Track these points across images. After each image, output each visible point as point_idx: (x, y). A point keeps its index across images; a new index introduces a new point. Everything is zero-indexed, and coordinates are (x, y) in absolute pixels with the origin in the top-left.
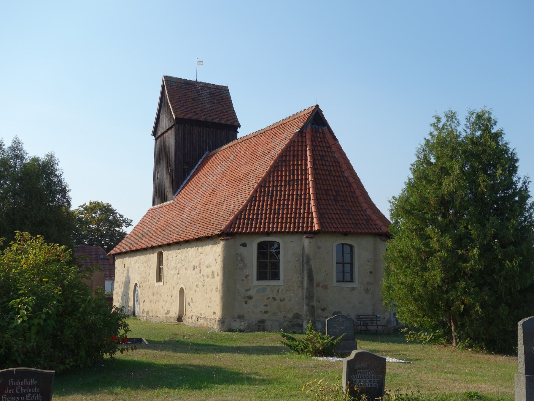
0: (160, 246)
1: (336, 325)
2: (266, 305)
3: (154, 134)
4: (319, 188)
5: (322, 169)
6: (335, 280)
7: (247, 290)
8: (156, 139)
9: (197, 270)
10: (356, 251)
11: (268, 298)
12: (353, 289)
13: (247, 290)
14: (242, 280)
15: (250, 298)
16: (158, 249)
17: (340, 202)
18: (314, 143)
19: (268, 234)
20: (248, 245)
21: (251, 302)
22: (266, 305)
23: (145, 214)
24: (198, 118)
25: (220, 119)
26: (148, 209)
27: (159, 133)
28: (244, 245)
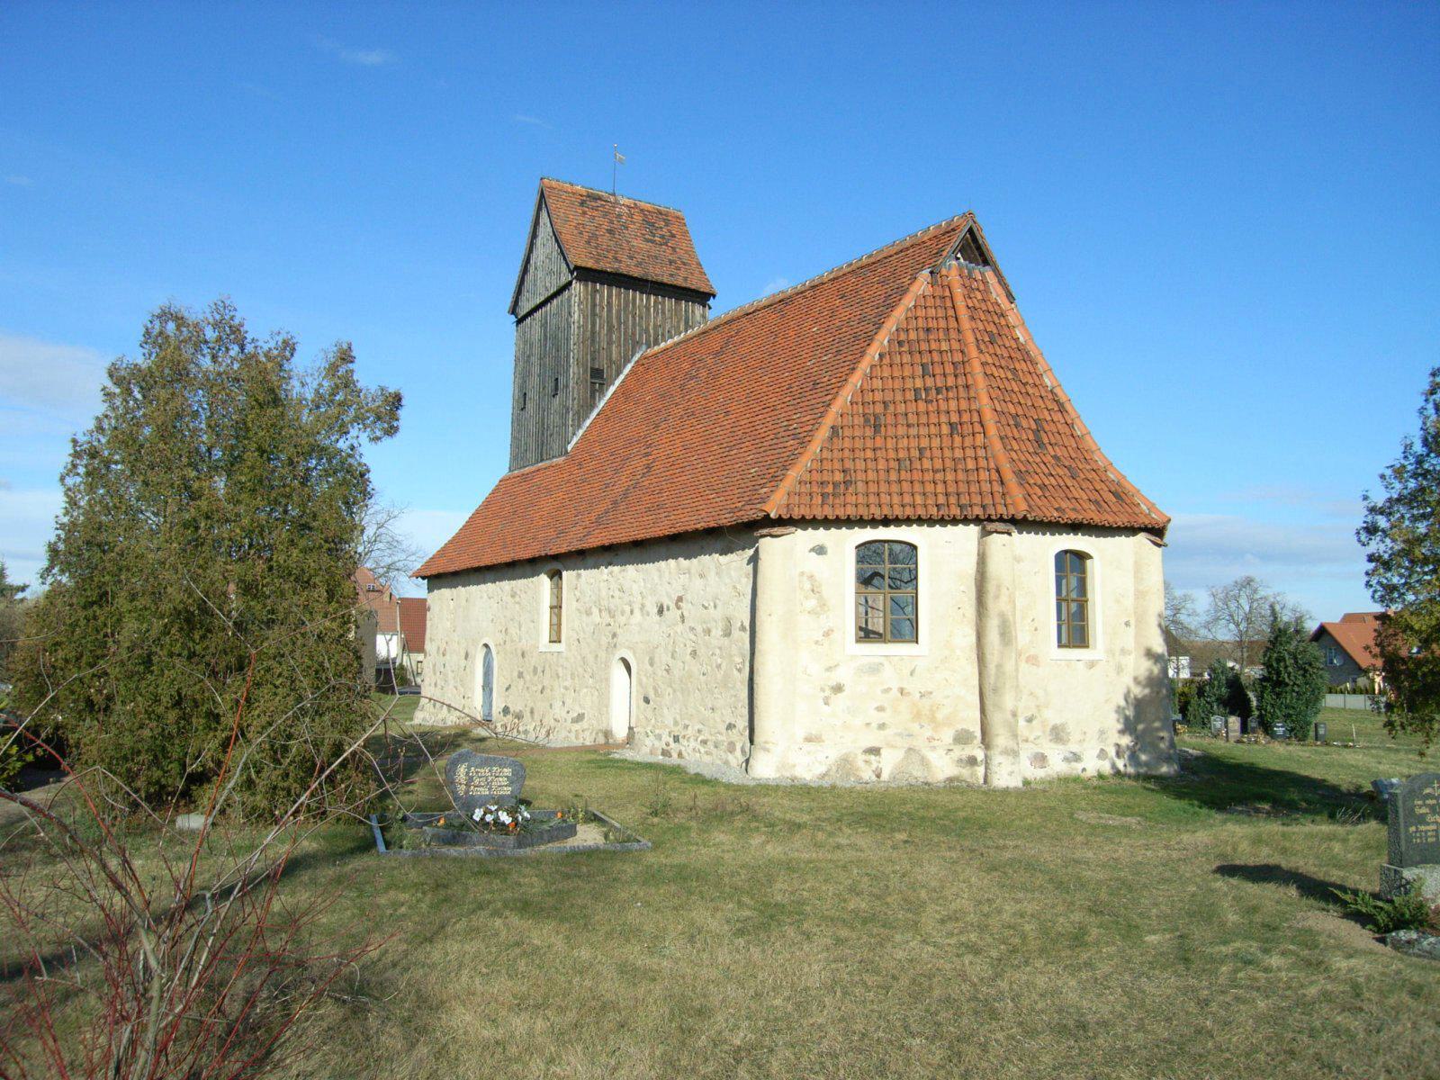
0: (556, 557)
1: (1424, 810)
2: (880, 709)
3: (513, 311)
4: (999, 409)
5: (997, 364)
6: (547, 638)
7: (829, 669)
8: (519, 322)
9: (672, 614)
10: (1094, 569)
11: (888, 690)
12: (1092, 665)
13: (829, 669)
14: (817, 642)
15: (838, 689)
16: (553, 563)
17: (1050, 448)
18: (969, 301)
19: (886, 522)
20: (829, 551)
21: (840, 701)
22: (880, 709)
23: (493, 487)
24: (624, 270)
25: (671, 275)
26: (500, 478)
27: (525, 307)
28: (820, 550)
